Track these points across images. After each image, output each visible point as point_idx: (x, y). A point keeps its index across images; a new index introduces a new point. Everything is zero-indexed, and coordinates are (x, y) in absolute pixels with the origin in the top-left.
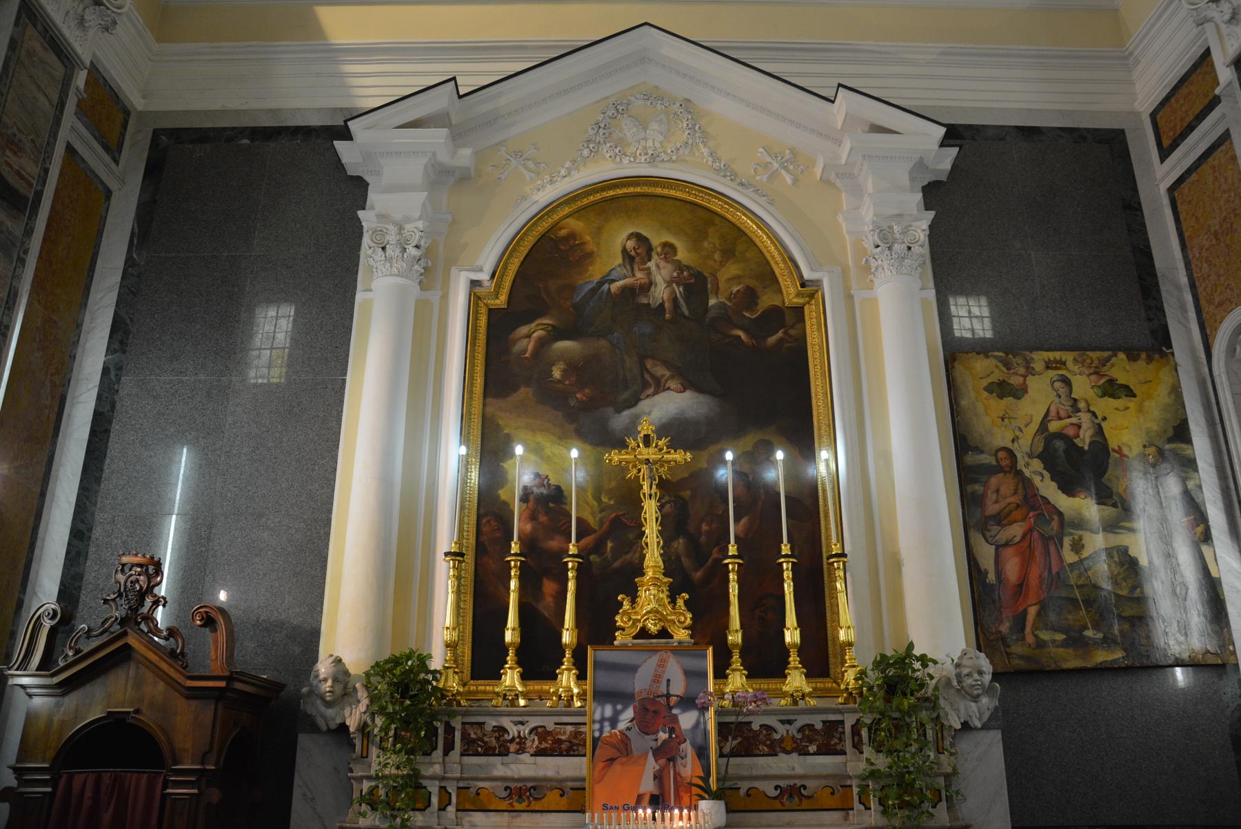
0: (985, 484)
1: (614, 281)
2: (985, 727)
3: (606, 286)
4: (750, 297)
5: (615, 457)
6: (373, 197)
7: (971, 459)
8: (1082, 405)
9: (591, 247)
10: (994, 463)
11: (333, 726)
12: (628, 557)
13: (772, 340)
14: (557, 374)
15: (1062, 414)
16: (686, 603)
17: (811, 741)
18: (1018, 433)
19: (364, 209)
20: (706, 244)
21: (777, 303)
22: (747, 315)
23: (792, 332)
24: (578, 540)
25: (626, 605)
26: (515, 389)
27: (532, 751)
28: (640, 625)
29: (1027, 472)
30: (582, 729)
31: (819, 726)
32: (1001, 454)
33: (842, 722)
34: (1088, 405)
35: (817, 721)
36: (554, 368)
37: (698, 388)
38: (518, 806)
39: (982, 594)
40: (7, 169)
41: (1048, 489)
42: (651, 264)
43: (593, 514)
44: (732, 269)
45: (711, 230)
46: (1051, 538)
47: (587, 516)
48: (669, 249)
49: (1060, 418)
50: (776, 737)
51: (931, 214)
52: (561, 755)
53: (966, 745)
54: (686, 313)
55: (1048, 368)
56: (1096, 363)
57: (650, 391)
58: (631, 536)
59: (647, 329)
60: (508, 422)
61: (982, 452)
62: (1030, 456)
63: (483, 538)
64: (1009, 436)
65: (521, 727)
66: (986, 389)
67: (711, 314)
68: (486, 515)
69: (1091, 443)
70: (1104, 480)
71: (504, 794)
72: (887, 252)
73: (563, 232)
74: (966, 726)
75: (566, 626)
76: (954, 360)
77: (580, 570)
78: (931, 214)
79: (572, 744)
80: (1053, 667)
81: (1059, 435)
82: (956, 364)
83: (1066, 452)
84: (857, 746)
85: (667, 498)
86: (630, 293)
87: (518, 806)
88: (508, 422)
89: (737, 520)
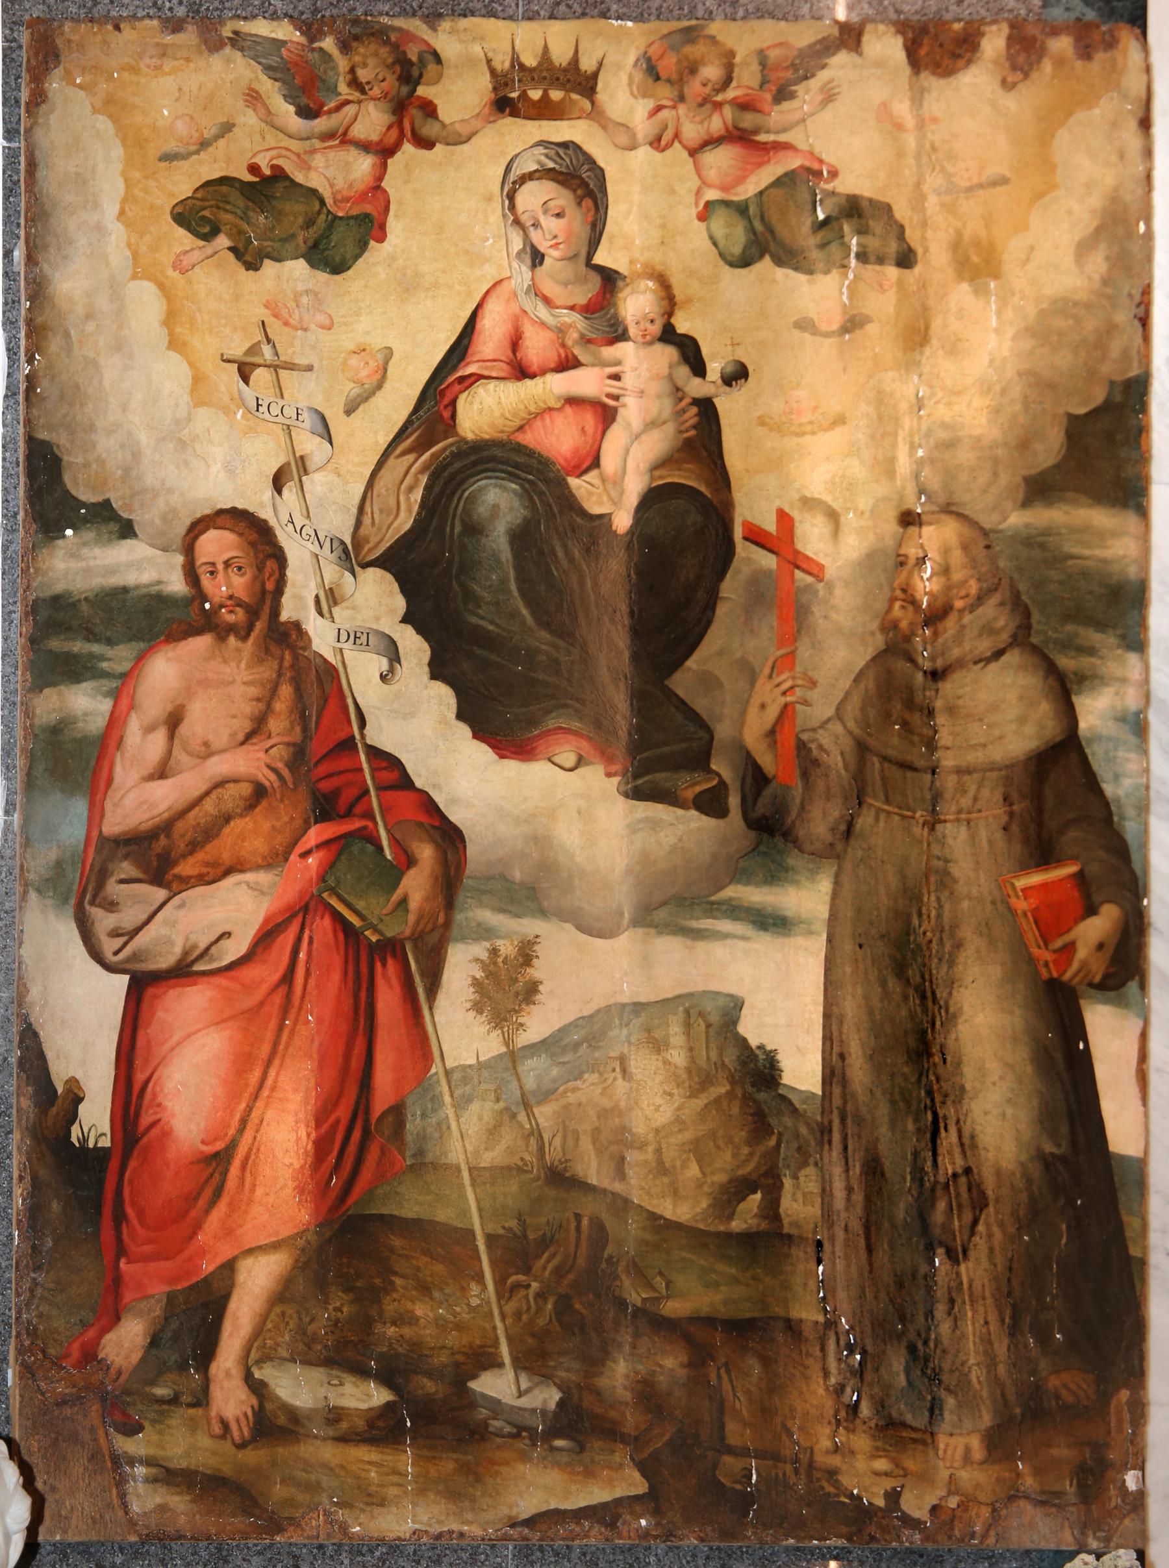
0: (122, 690)
8: (637, 305)
10: (177, 585)
15: (537, 346)
18: (310, 445)
29: (322, 637)
32: (216, 545)
41: (412, 719)
46: (392, 948)
49: (521, 372)
55: (503, 105)
56: (747, 78)
61: (127, 530)
62: (352, 556)
69: (652, 499)
70: (682, 683)
81: (506, 456)
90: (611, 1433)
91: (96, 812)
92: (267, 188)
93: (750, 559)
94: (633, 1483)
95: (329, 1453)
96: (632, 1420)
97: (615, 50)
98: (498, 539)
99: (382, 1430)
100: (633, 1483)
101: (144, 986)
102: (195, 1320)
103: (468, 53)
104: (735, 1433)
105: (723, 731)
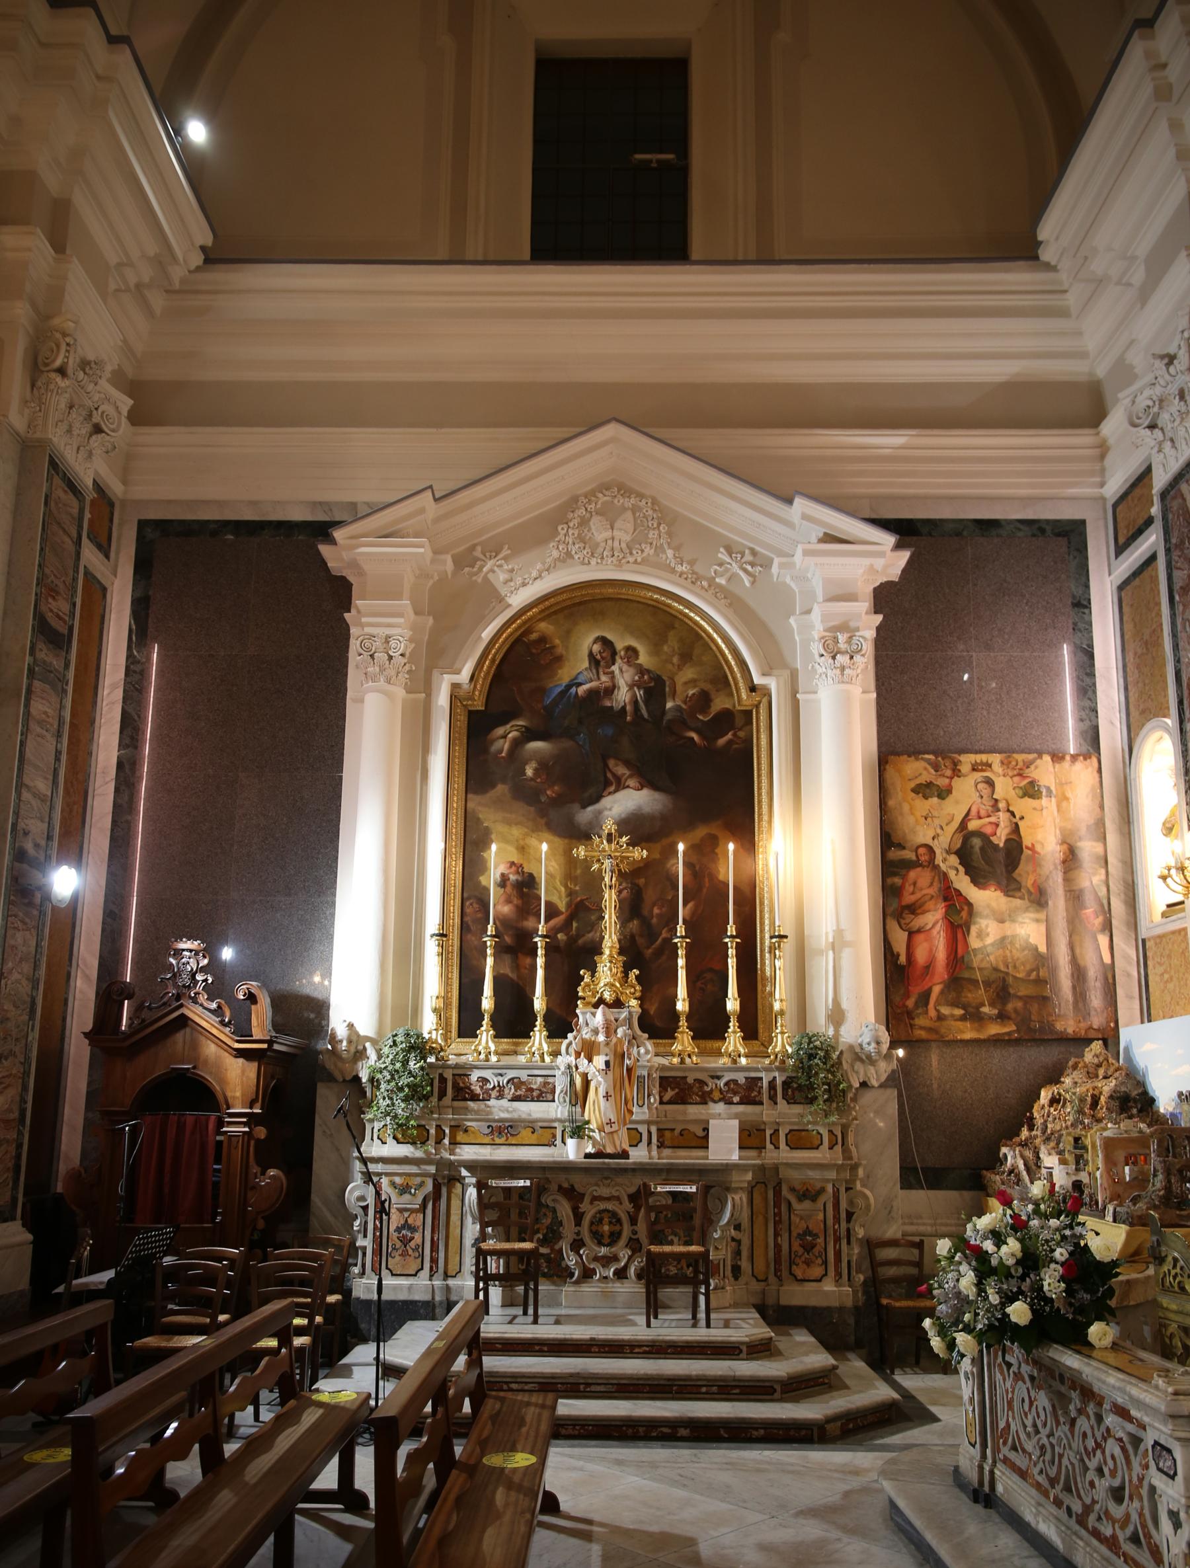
0: (904, 877)
1: (580, 684)
2: (882, 1086)
3: (573, 690)
4: (704, 700)
5: (581, 852)
6: (358, 603)
7: (894, 854)
8: (1002, 805)
9: (560, 650)
10: (914, 858)
11: (348, 1078)
12: (590, 935)
13: (721, 742)
14: (529, 772)
15: (983, 813)
16: (637, 977)
17: (735, 1093)
18: (939, 831)
19: (349, 611)
20: (665, 648)
21: (728, 706)
22: (701, 717)
23: (741, 734)
24: (546, 921)
25: (587, 979)
26: (493, 786)
27: (509, 1097)
28: (598, 996)
29: (943, 867)
30: (550, 1080)
31: (742, 1081)
32: (922, 851)
33: (761, 1079)
34: (1008, 805)
35: (741, 1078)
36: (527, 767)
37: (655, 787)
38: (498, 1141)
39: (897, 974)
40: (50, 614)
41: (962, 882)
42: (615, 668)
43: (560, 898)
44: (689, 673)
45: (671, 633)
46: (960, 926)
47: (555, 899)
48: (632, 652)
49: (980, 818)
50: (707, 1089)
51: (879, 618)
52: (532, 1100)
53: (867, 1097)
54: (646, 715)
55: (974, 770)
56: (1020, 765)
57: (612, 789)
58: (593, 918)
59: (610, 731)
60: (489, 817)
61: (904, 848)
62: (948, 852)
63: (466, 919)
64: (931, 833)
65: (500, 1079)
66: (913, 790)
67: (668, 717)
68: (469, 898)
69: (1007, 841)
70: (1015, 875)
71: (488, 1131)
72: (831, 661)
73: (534, 636)
74: (864, 1085)
75: (730, 995)
76: (887, 762)
77: (548, 948)
78: (879, 618)
79: (542, 1092)
80: (950, 1037)
81: (978, 833)
82: (887, 767)
83: (982, 849)
84: (773, 1098)
85: (624, 885)
86: (594, 695)
87: (498, 1141)
88: (489, 817)
89: (685, 905)
90: (1009, 1018)
91: (900, 902)
92: (929, 785)
93: (1026, 852)
94: (1014, 1028)
95: (953, 1023)
96: (1013, 1016)
97: (995, 759)
98: (977, 849)
99: (963, 1018)
100: (1014, 1028)
101: (911, 934)
102: (926, 995)
103: (967, 760)
104: (1033, 1017)
105: (1023, 884)
